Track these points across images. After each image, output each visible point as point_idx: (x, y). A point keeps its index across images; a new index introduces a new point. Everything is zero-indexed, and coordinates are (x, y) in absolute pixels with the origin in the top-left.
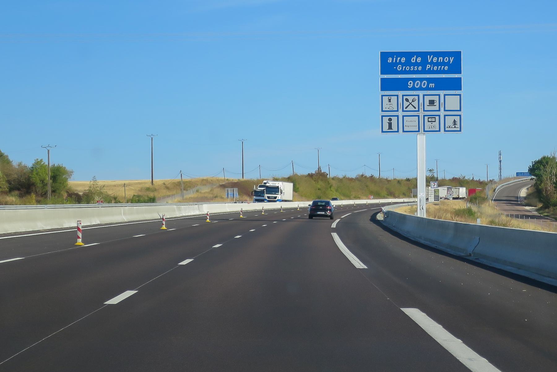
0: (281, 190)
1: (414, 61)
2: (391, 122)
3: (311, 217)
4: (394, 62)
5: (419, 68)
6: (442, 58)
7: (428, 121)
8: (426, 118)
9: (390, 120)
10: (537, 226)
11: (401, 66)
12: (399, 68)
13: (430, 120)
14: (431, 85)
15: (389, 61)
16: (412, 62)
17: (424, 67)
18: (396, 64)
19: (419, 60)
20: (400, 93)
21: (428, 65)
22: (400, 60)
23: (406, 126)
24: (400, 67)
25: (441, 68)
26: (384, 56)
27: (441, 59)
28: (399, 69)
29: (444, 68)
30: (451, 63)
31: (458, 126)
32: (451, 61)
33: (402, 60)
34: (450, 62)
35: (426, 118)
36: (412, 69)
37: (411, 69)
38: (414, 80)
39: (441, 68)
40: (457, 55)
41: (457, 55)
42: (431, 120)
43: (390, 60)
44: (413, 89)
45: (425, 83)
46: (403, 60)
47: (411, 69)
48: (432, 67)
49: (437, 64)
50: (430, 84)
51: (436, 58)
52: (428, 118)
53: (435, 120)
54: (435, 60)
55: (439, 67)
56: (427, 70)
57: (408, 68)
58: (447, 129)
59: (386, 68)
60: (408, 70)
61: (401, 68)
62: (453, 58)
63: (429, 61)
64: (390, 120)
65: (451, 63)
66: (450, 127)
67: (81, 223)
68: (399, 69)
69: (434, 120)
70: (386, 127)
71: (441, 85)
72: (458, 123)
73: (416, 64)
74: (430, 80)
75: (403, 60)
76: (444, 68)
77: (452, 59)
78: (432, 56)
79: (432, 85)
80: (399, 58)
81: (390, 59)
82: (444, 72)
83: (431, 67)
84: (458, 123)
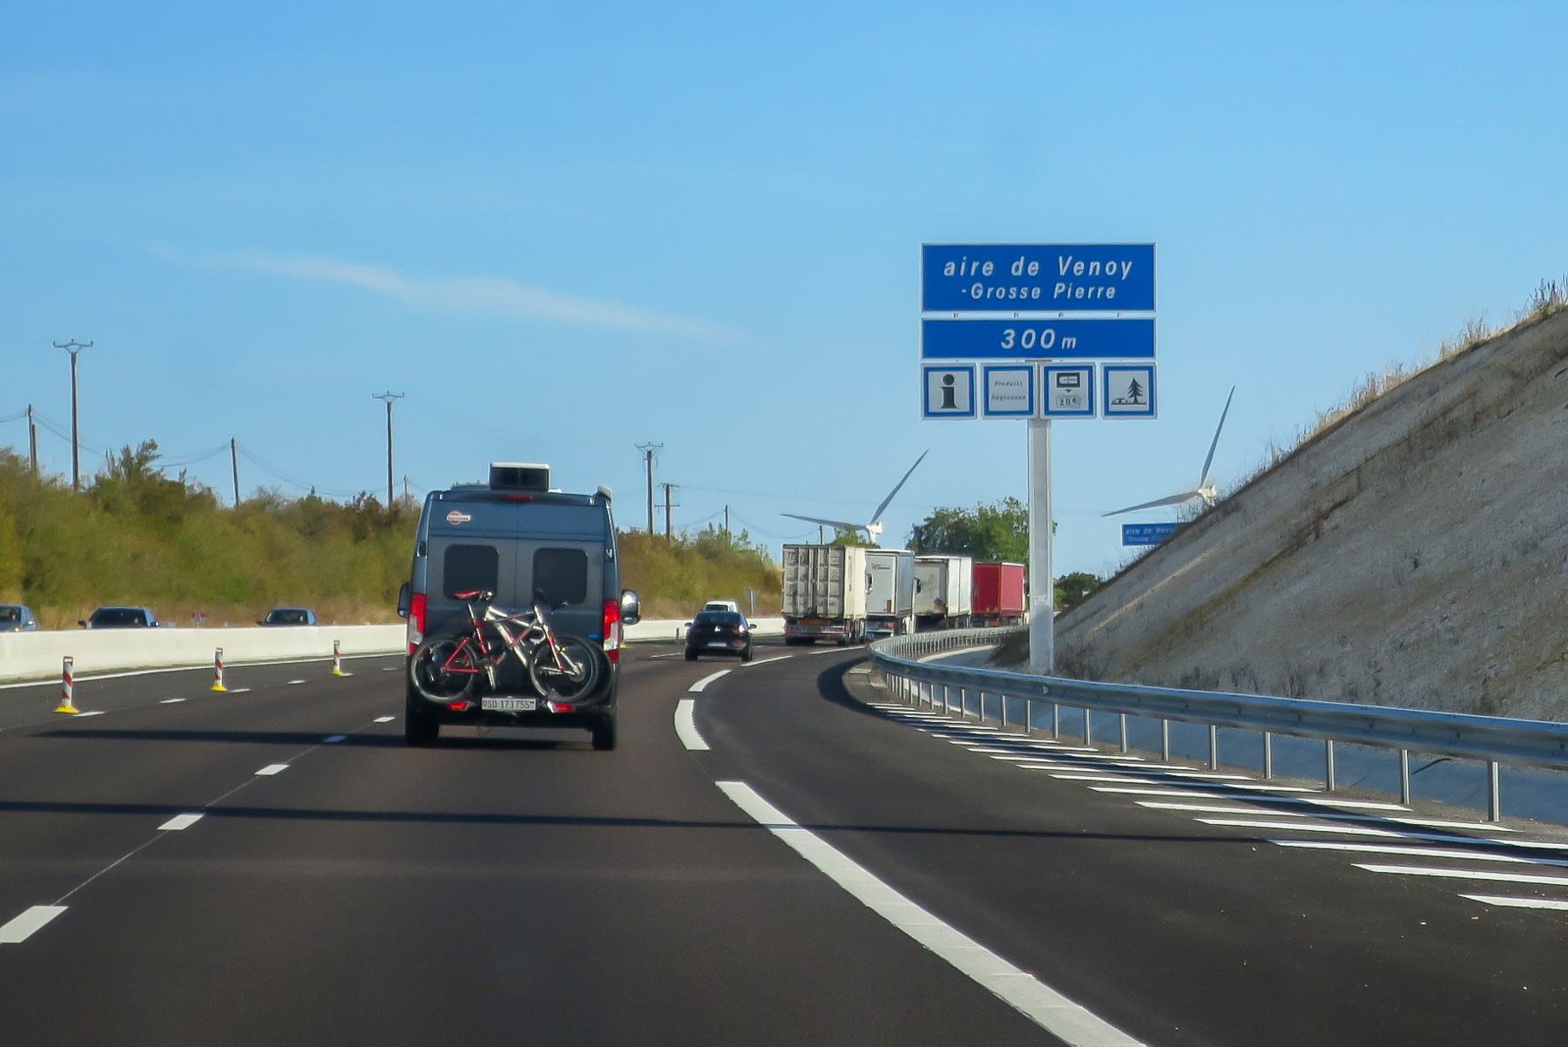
0: (611, 690)
1: (1020, 273)
4: (962, 274)
7: (1059, 385)
8: (1053, 375)
9: (949, 379)
12: (977, 291)
13: (1063, 380)
14: (1066, 342)
18: (968, 281)
19: (1034, 268)
20: (979, 364)
21: (1058, 285)
22: (979, 269)
23: (993, 397)
24: (978, 288)
25: (1095, 292)
26: (935, 256)
27: (1095, 267)
29: (1104, 293)
30: (1124, 278)
32: (1125, 273)
33: (984, 268)
35: (1053, 375)
36: (1012, 295)
37: (1010, 297)
38: (1020, 326)
39: (1095, 292)
40: (1142, 256)
41: (1142, 256)
42: (1066, 382)
43: (950, 269)
44: (1017, 351)
45: (1049, 336)
46: (988, 268)
47: (1003, 344)
49: (1085, 280)
50: (1064, 340)
54: (1079, 268)
55: (1091, 290)
56: (1055, 297)
57: (1001, 293)
58: (1112, 408)
59: (938, 290)
60: (1002, 297)
61: (981, 292)
62: (1130, 263)
63: (1062, 273)
64: (949, 379)
65: (1124, 278)
66: (1123, 401)
67: (71, 663)
69: (1076, 382)
71: (1097, 340)
73: (1026, 280)
74: (1063, 328)
75: (988, 268)
76: (1104, 293)
77: (1063, 267)
78: (1070, 258)
79: (1070, 342)
80: (975, 265)
82: (1104, 304)
83: (1066, 291)
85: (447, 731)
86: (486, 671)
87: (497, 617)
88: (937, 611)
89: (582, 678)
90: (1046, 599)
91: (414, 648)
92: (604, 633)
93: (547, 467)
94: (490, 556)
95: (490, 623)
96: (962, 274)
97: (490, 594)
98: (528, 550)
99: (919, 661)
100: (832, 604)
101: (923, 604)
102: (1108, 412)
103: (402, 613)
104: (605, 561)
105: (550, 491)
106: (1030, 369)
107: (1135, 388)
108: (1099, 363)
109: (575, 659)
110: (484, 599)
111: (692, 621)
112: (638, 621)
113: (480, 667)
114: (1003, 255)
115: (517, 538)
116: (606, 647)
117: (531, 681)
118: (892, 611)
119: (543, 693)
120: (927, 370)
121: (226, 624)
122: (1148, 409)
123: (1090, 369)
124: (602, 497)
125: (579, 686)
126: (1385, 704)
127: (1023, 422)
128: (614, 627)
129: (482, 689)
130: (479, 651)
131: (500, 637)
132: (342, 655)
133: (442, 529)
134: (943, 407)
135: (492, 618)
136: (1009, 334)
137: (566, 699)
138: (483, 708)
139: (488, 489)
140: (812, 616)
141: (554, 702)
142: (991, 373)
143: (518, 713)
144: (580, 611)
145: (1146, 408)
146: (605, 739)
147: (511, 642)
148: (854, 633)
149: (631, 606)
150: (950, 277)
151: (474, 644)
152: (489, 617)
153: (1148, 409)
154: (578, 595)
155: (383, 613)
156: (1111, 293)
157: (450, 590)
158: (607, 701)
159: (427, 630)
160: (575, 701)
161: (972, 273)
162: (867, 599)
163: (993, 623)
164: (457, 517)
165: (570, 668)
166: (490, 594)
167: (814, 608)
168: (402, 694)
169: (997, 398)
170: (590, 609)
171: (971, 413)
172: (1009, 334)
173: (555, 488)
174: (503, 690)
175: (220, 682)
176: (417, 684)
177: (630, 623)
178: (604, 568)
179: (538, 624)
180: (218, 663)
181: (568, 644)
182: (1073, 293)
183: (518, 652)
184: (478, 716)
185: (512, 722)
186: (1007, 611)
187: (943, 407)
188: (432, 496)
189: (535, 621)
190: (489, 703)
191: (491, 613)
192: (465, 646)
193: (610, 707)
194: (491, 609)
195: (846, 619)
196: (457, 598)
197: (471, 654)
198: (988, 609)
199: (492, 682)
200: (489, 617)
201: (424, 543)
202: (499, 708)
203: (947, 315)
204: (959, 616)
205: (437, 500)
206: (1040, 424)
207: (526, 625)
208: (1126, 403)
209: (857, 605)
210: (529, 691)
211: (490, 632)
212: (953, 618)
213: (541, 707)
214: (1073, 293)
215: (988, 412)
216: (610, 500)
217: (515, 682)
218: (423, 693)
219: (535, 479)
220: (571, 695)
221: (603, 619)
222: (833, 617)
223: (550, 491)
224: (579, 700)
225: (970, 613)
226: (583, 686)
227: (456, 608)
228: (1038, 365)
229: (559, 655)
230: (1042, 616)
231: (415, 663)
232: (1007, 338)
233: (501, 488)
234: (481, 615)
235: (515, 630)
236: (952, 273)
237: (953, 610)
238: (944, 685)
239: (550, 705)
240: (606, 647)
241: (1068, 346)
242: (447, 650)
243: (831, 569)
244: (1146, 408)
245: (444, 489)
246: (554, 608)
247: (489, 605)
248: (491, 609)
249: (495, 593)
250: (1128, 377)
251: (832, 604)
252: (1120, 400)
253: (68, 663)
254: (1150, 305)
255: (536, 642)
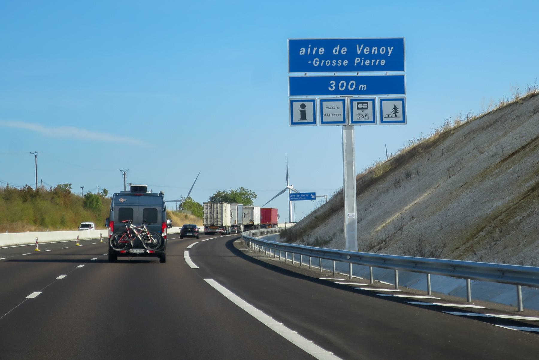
0: (164, 248)
1: (337, 53)
2: (305, 110)
3: (182, 237)
4: (309, 53)
5: (344, 63)
6: (376, 48)
7: (358, 108)
8: (355, 103)
9: (303, 106)
10: (526, 105)
11: (318, 60)
12: (316, 62)
13: (360, 106)
14: (361, 87)
15: (302, 53)
16: (335, 53)
17: (351, 62)
18: (312, 57)
19: (344, 51)
20: (318, 98)
21: (357, 59)
22: (317, 51)
23: (325, 115)
24: (316, 61)
25: (375, 63)
27: (375, 49)
28: (316, 64)
29: (379, 63)
30: (389, 55)
31: (400, 114)
32: (390, 52)
33: (320, 51)
34: (388, 53)
35: (355, 103)
37: (333, 65)
38: (338, 79)
39: (375, 63)
42: (362, 107)
43: (302, 52)
45: (352, 84)
46: (321, 51)
47: (330, 88)
48: (363, 61)
49: (370, 56)
50: (360, 86)
51: (368, 48)
52: (357, 103)
53: (368, 106)
54: (367, 51)
55: (373, 61)
57: (328, 63)
58: (384, 119)
61: (318, 63)
62: (392, 48)
63: (359, 53)
64: (303, 106)
65: (389, 55)
66: (390, 116)
68: (316, 64)
69: (366, 107)
70: (297, 117)
72: (400, 110)
73: (340, 57)
74: (359, 80)
75: (321, 51)
76: (379, 63)
78: (362, 45)
79: (363, 87)
80: (315, 49)
81: (303, 50)
83: (361, 62)
84: (400, 110)
85: (119, 258)
86: (130, 242)
87: (133, 227)
88: (250, 224)
89: (157, 244)
90: (353, 215)
91: (111, 236)
92: (162, 231)
93: (146, 186)
94: (131, 210)
95: (131, 229)
96: (309, 53)
97: (131, 221)
98: (141, 209)
99: (256, 238)
100: (219, 222)
101: (246, 222)
102: (382, 122)
103: (106, 226)
104: (162, 212)
105: (147, 192)
106: (343, 101)
107: (395, 109)
108: (377, 97)
109: (155, 238)
110: (130, 222)
111: (182, 227)
112: (171, 227)
113: (129, 241)
114: (329, 44)
115: (138, 206)
116: (163, 235)
117: (143, 245)
118: (236, 224)
119: (146, 248)
120: (292, 102)
121: (7, 232)
122: (402, 120)
123: (373, 100)
124: (161, 194)
125: (156, 246)
126: (506, 264)
127: (340, 127)
128: (165, 229)
129: (130, 247)
130: (128, 237)
131: (134, 233)
132: (103, 238)
133: (118, 204)
134: (300, 120)
135: (132, 228)
136: (333, 83)
137: (153, 249)
138: (130, 252)
139: (130, 192)
140: (213, 225)
141: (149, 250)
142: (324, 103)
143: (139, 253)
144: (155, 225)
145: (401, 119)
146: (163, 260)
147: (137, 234)
148: (227, 231)
149: (169, 223)
150: (302, 55)
151: (127, 235)
152: (131, 227)
153: (402, 120)
154: (155, 221)
155: (33, 228)
156: (383, 62)
157: (120, 220)
158: (163, 250)
159: (114, 231)
160: (155, 250)
161: (314, 53)
162: (231, 220)
163: (269, 227)
164: (122, 200)
165: (154, 241)
166: (131, 221)
167: (213, 223)
168: (108, 249)
169: (327, 115)
170: (158, 225)
171: (314, 123)
172: (333, 83)
173: (149, 192)
174: (135, 247)
175: (38, 248)
176: (112, 245)
177: (169, 228)
178: (162, 213)
179: (144, 229)
180: (37, 242)
181: (153, 234)
182: (364, 62)
183: (139, 236)
184: (128, 254)
185: (138, 256)
186: (274, 223)
187: (300, 120)
188: (115, 195)
189: (144, 228)
190: (132, 251)
191: (132, 226)
192: (125, 235)
193: (164, 251)
194: (132, 225)
195: (224, 226)
196: (122, 222)
197: (126, 237)
198: (267, 223)
199: (132, 245)
200: (131, 227)
201: (113, 207)
202: (134, 252)
203: (301, 74)
204: (257, 225)
205: (116, 195)
206: (349, 128)
207: (141, 229)
208: (391, 117)
209: (228, 222)
210: (143, 248)
211: (132, 231)
212: (255, 226)
213: (146, 252)
214: (364, 62)
215: (323, 122)
216: (163, 195)
217: (138, 245)
218: (113, 248)
219: (143, 189)
220: (153, 248)
221: (162, 228)
222: (220, 225)
223: (147, 192)
224: (156, 250)
225: (260, 224)
226: (157, 246)
227: (122, 225)
228: (347, 98)
229: (150, 237)
230: (351, 224)
231: (111, 240)
232: (332, 85)
233: (134, 192)
234: (129, 227)
235: (138, 231)
236: (304, 54)
237: (255, 223)
238: (279, 250)
239: (148, 251)
240: (163, 235)
241: (362, 89)
242: (120, 236)
243: (218, 215)
244: (401, 119)
245: (118, 193)
246: (149, 225)
247: (131, 224)
248: (132, 225)
249: (132, 221)
250: (392, 104)
251: (219, 222)
252: (388, 115)
253: (37, 239)
254: (402, 68)
255: (144, 234)
